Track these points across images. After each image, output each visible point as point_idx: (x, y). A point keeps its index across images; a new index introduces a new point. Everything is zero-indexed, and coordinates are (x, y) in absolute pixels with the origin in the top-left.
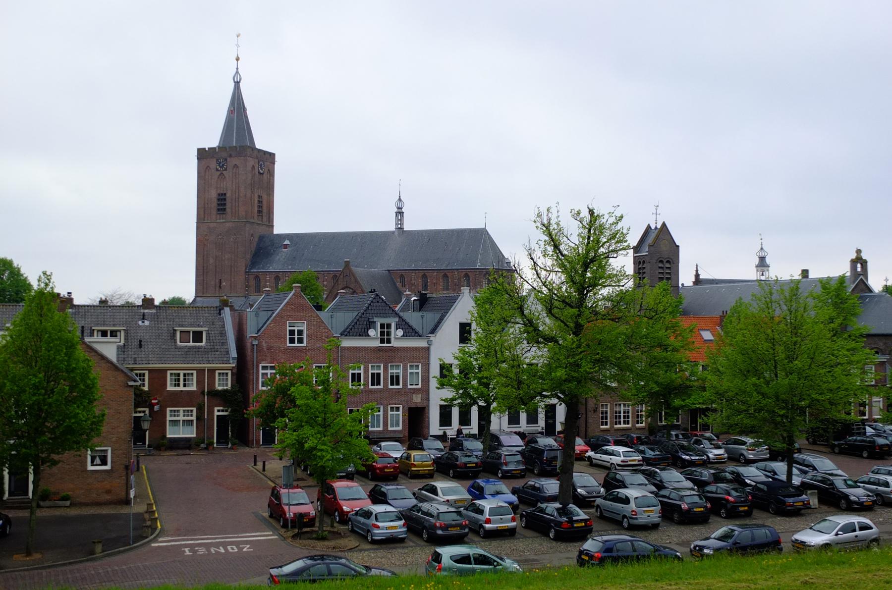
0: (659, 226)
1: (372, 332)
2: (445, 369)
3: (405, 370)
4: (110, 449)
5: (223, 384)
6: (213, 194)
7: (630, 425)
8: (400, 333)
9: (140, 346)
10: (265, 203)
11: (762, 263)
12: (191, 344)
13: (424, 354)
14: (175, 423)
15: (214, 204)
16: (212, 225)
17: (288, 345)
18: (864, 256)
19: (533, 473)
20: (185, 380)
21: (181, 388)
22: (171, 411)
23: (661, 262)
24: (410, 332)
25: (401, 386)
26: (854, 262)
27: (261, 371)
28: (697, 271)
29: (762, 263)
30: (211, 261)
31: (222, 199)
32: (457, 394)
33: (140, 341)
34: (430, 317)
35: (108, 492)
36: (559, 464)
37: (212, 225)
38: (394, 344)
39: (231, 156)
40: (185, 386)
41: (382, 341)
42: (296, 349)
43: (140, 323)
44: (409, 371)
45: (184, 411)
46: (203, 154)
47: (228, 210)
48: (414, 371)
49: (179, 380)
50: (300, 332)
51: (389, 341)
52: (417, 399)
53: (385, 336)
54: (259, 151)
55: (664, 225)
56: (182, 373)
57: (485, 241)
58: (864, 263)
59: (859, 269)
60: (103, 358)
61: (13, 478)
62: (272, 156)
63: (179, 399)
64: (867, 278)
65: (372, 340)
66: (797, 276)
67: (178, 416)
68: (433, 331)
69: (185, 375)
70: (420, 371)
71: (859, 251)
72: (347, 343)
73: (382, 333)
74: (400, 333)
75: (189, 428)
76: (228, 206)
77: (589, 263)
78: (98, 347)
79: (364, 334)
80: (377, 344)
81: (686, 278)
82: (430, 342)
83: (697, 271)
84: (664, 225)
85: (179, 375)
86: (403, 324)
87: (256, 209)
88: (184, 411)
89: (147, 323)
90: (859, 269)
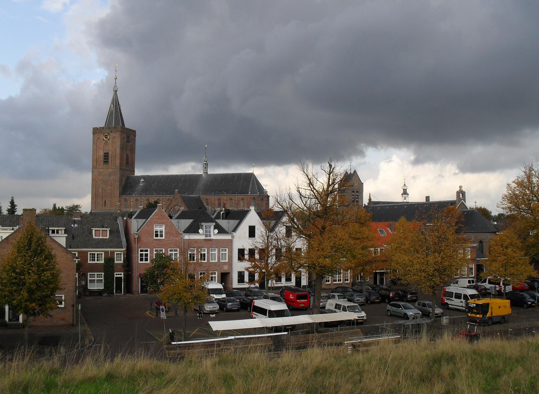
0: (352, 172)
1: (201, 231)
2: (241, 252)
3: (219, 252)
4: (63, 296)
5: (119, 261)
6: (101, 153)
7: (342, 282)
8: (216, 231)
9: (73, 238)
10: (130, 158)
11: (405, 193)
12: (101, 237)
13: (229, 244)
14: (92, 281)
15: (102, 159)
16: (101, 170)
17: (164, 238)
18: (464, 189)
19: (523, 307)
20: (98, 257)
21: (96, 262)
22: (90, 274)
23: (353, 192)
24: (222, 231)
25: (206, 261)
26: (458, 193)
27: (140, 253)
28: (370, 197)
29: (405, 193)
30: (100, 190)
31: (106, 155)
32: (251, 265)
33: (73, 236)
34: (233, 223)
35: (63, 319)
36: (60, 306)
37: (101, 170)
38: (213, 237)
39: (111, 132)
40: (98, 260)
41: (206, 236)
42: (159, 240)
43: (72, 225)
44: (221, 252)
45: (97, 274)
46: (96, 131)
47: (110, 162)
48: (224, 252)
49: (94, 257)
50: (161, 232)
51: (210, 236)
52: (226, 268)
53: (207, 234)
54: (127, 129)
55: (355, 172)
56: (96, 253)
57: (253, 180)
58: (463, 193)
59: (461, 197)
60: (60, 245)
61: (11, 311)
62: (134, 132)
63: (95, 268)
64: (465, 201)
65: (200, 236)
66: (424, 200)
67: (94, 277)
68: (235, 230)
69: (98, 255)
70: (227, 252)
71: (460, 187)
72: (187, 237)
73: (206, 232)
74: (216, 231)
75: (101, 284)
76: (110, 160)
77: (329, 194)
78: (55, 239)
79: (196, 232)
80: (203, 237)
81: (365, 202)
82: (233, 237)
83: (370, 197)
84: (355, 172)
85: (94, 254)
86: (217, 227)
87: (125, 162)
88: (97, 274)
89: (76, 225)
90: (461, 197)
